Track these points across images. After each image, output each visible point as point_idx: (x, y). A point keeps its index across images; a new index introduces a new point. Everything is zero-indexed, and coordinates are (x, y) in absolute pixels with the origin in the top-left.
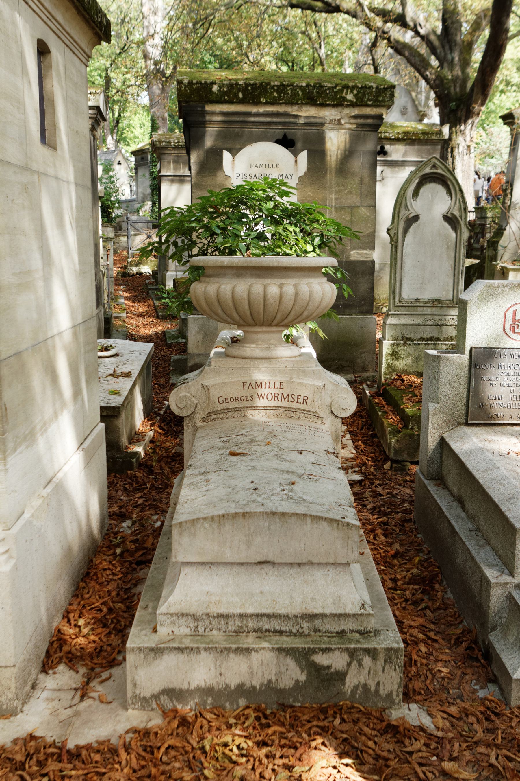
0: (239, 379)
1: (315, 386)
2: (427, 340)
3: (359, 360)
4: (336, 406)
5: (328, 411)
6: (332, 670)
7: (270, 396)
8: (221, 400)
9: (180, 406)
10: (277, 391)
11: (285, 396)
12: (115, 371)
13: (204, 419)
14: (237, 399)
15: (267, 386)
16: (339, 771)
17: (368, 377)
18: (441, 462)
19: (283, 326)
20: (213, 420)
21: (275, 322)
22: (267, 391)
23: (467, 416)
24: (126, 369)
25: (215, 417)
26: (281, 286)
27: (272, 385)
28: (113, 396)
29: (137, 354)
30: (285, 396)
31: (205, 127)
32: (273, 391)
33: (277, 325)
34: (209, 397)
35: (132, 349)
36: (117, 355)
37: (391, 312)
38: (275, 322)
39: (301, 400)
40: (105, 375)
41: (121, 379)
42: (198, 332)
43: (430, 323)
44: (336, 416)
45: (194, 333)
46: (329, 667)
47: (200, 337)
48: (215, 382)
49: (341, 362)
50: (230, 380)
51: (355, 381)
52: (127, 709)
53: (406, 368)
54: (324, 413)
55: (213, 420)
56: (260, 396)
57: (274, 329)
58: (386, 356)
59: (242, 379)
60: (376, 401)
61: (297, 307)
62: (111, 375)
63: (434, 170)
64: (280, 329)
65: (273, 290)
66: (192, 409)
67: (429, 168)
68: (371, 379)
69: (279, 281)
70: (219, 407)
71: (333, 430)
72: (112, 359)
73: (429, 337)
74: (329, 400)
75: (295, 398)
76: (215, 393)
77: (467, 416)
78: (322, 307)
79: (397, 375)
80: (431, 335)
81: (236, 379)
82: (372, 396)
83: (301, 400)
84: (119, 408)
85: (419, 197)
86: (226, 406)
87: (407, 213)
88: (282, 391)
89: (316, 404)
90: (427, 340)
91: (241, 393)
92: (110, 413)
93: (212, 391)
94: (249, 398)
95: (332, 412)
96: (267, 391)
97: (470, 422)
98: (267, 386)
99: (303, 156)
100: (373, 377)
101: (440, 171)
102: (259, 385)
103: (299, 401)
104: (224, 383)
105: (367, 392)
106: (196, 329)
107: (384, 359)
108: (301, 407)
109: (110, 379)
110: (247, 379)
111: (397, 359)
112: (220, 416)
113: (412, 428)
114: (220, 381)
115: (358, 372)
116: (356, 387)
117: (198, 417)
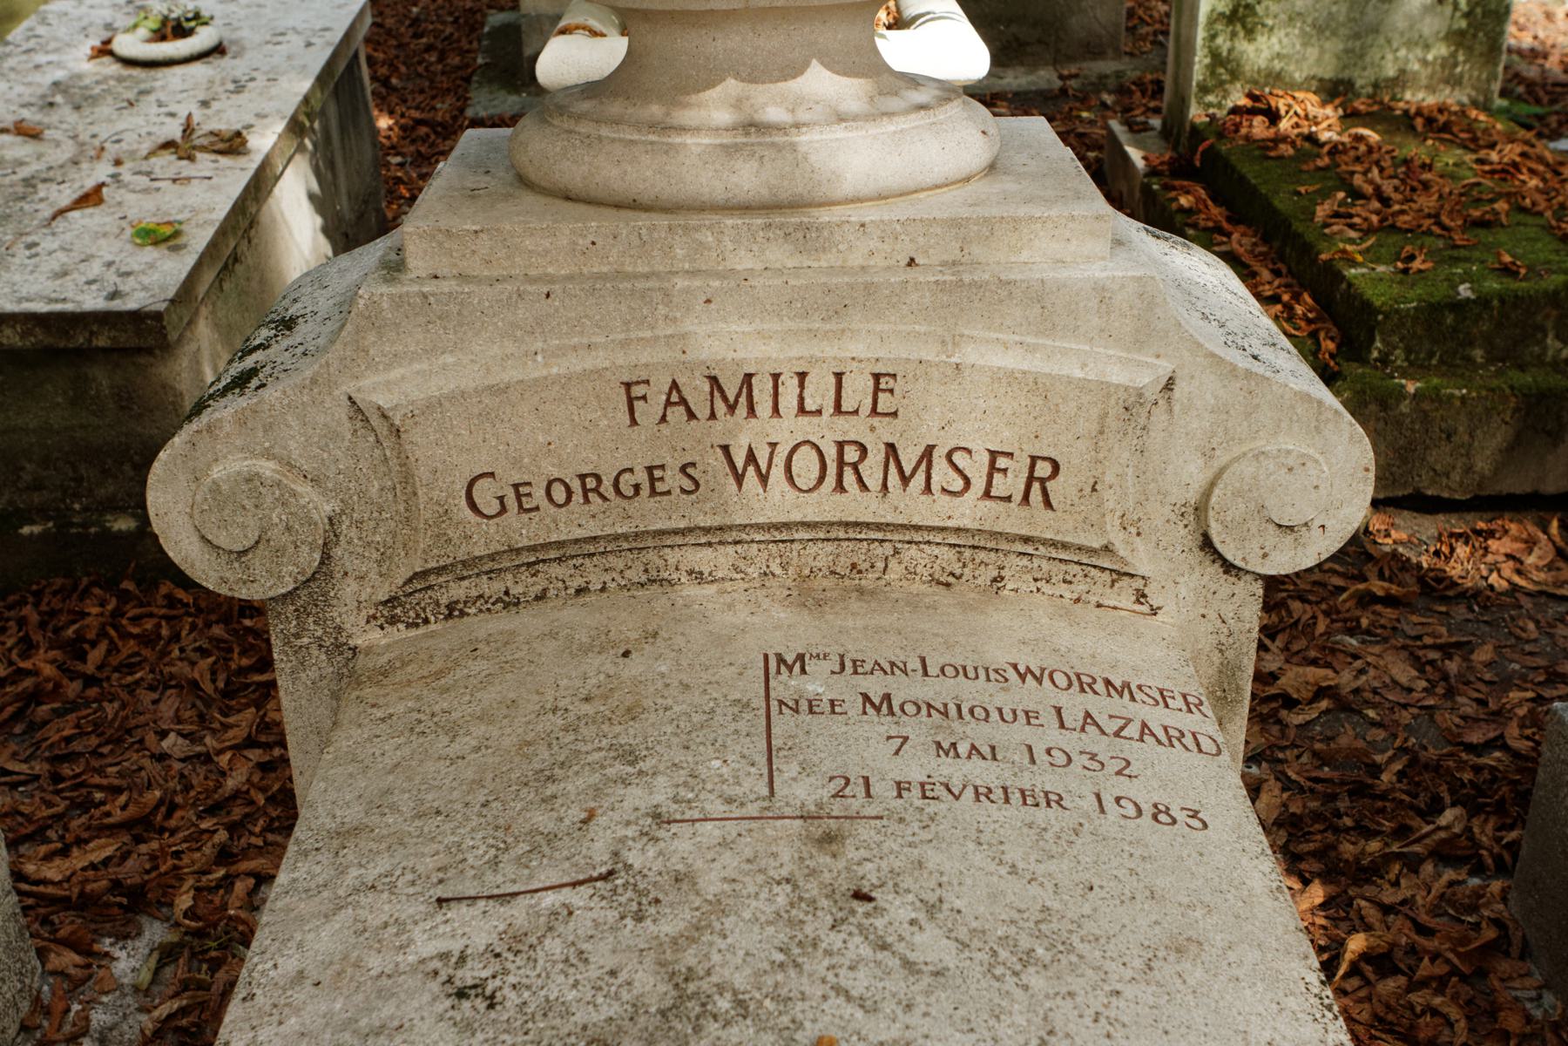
0: (599, 360)
1: (1106, 389)
3: (1074, 22)
4: (1238, 509)
5: (1183, 536)
7: (806, 465)
8: (486, 495)
9: (222, 539)
10: (854, 429)
12: (188, 129)
13: (391, 611)
14: (590, 484)
15: (789, 401)
17: (1103, 77)
20: (453, 611)
22: (789, 429)
24: (226, 118)
25: (458, 591)
27: (819, 393)
28: (150, 254)
29: (297, 41)
30: (909, 459)
32: (827, 431)
34: (407, 478)
35: (282, 24)
36: (218, 50)
40: (145, 147)
41: (205, 162)
44: (1228, 567)
48: (438, 386)
49: (1014, 29)
50: (535, 370)
51: (1063, 91)
53: (1277, 65)
54: (1161, 557)
55: (453, 611)
56: (746, 467)
58: (1211, 22)
59: (625, 362)
60: (1184, 201)
62: (169, 145)
66: (310, 559)
68: (1112, 83)
70: (483, 538)
71: (1207, 643)
72: (197, 69)
74: (1190, 475)
75: (976, 468)
76: (445, 460)
79: (1250, 96)
81: (577, 364)
82: (1153, 172)
83: (1011, 483)
84: (157, 316)
86: (523, 530)
88: (886, 431)
89: (1110, 498)
91: (616, 448)
92: (127, 338)
93: (420, 442)
94: (673, 480)
95: (1207, 544)
96: (789, 429)
98: (789, 401)
100: (1119, 74)
102: (735, 394)
103: (1000, 485)
104: (500, 390)
105: (1136, 155)
107: (1201, 34)
108: (1013, 520)
109: (166, 164)
110: (653, 359)
111: (1250, 34)
112: (494, 588)
113: (1384, 360)
114: (470, 379)
115: (1071, 59)
116: (1069, 117)
117: (351, 602)
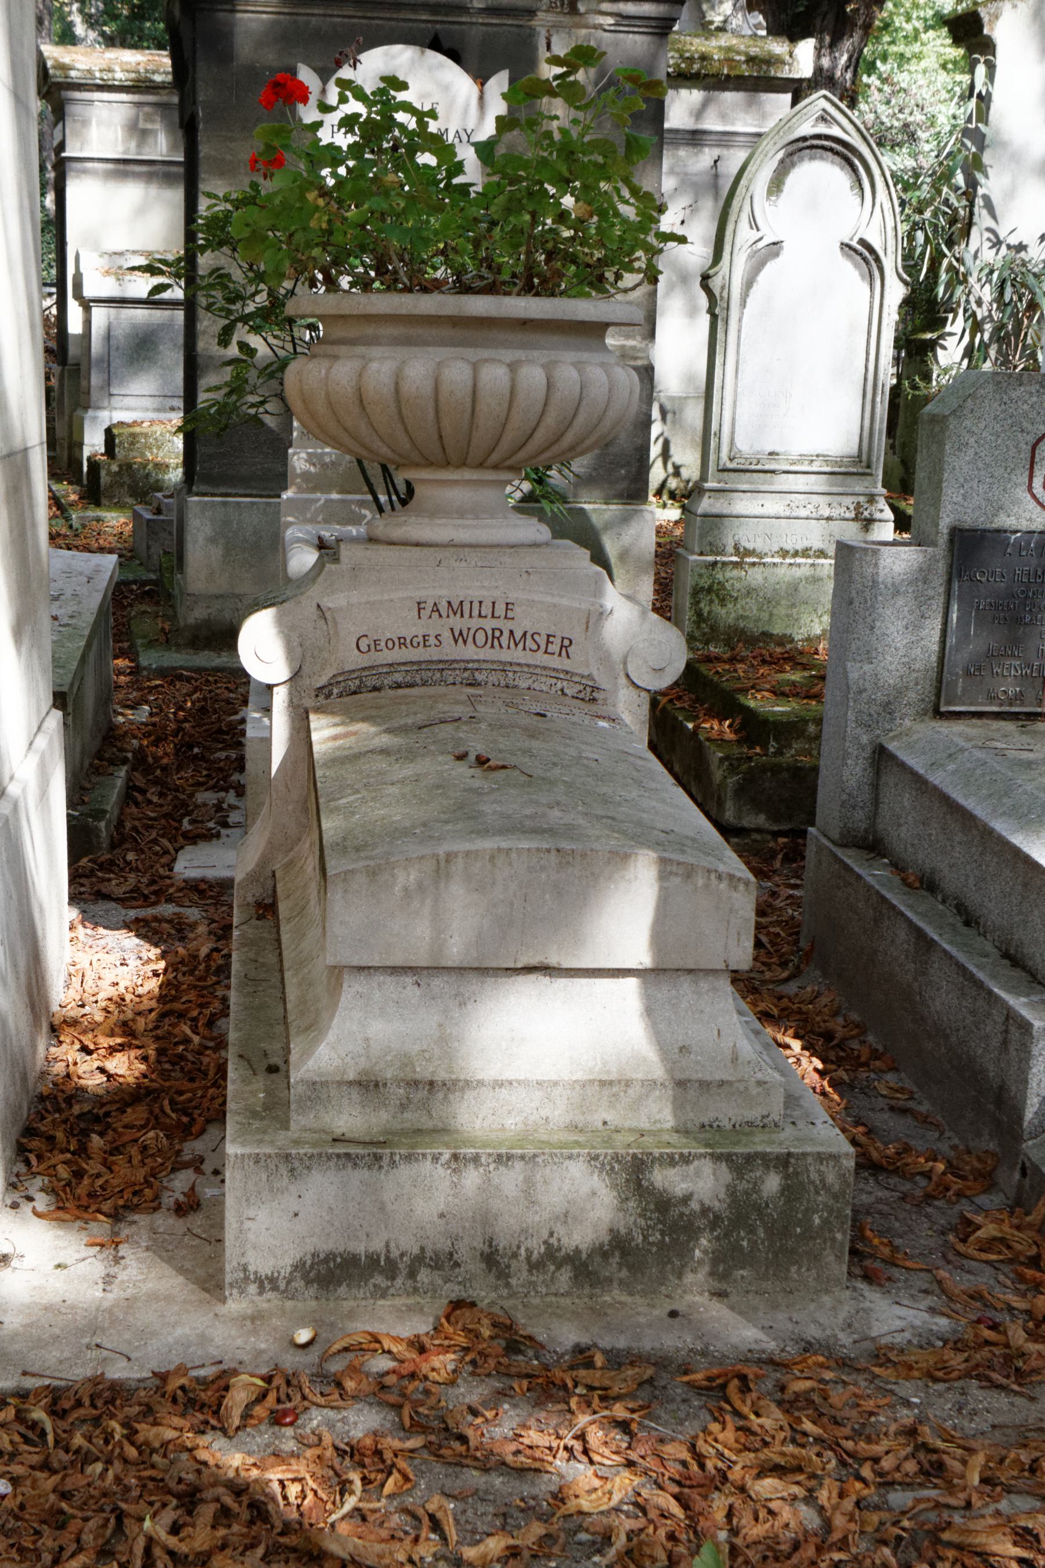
2: (796, 554)
6: (695, 1206)
7: (481, 637)
8: (364, 644)
11: (518, 635)
14: (402, 642)
15: (475, 613)
16: (791, 1319)
18: (876, 802)
19: (511, 468)
21: (495, 457)
23: (938, 695)
26: (513, 367)
27: (486, 610)
30: (518, 635)
31: (234, 11)
33: (496, 467)
37: (708, 485)
38: (495, 457)
39: (554, 648)
42: (212, 540)
43: (804, 513)
44: (638, 687)
45: (201, 541)
46: (686, 1199)
47: (216, 552)
52: (223, 1300)
57: (490, 475)
61: (551, 419)
63: (822, 129)
64: (504, 476)
65: (495, 376)
67: (811, 121)
69: (509, 355)
73: (799, 547)
77: (938, 695)
78: (612, 414)
80: (806, 544)
83: (554, 648)
85: (784, 195)
87: (754, 235)
90: (796, 554)
94: (432, 641)
97: (943, 709)
98: (475, 613)
99: (499, 82)
101: (835, 131)
106: (208, 530)
108: (554, 662)
